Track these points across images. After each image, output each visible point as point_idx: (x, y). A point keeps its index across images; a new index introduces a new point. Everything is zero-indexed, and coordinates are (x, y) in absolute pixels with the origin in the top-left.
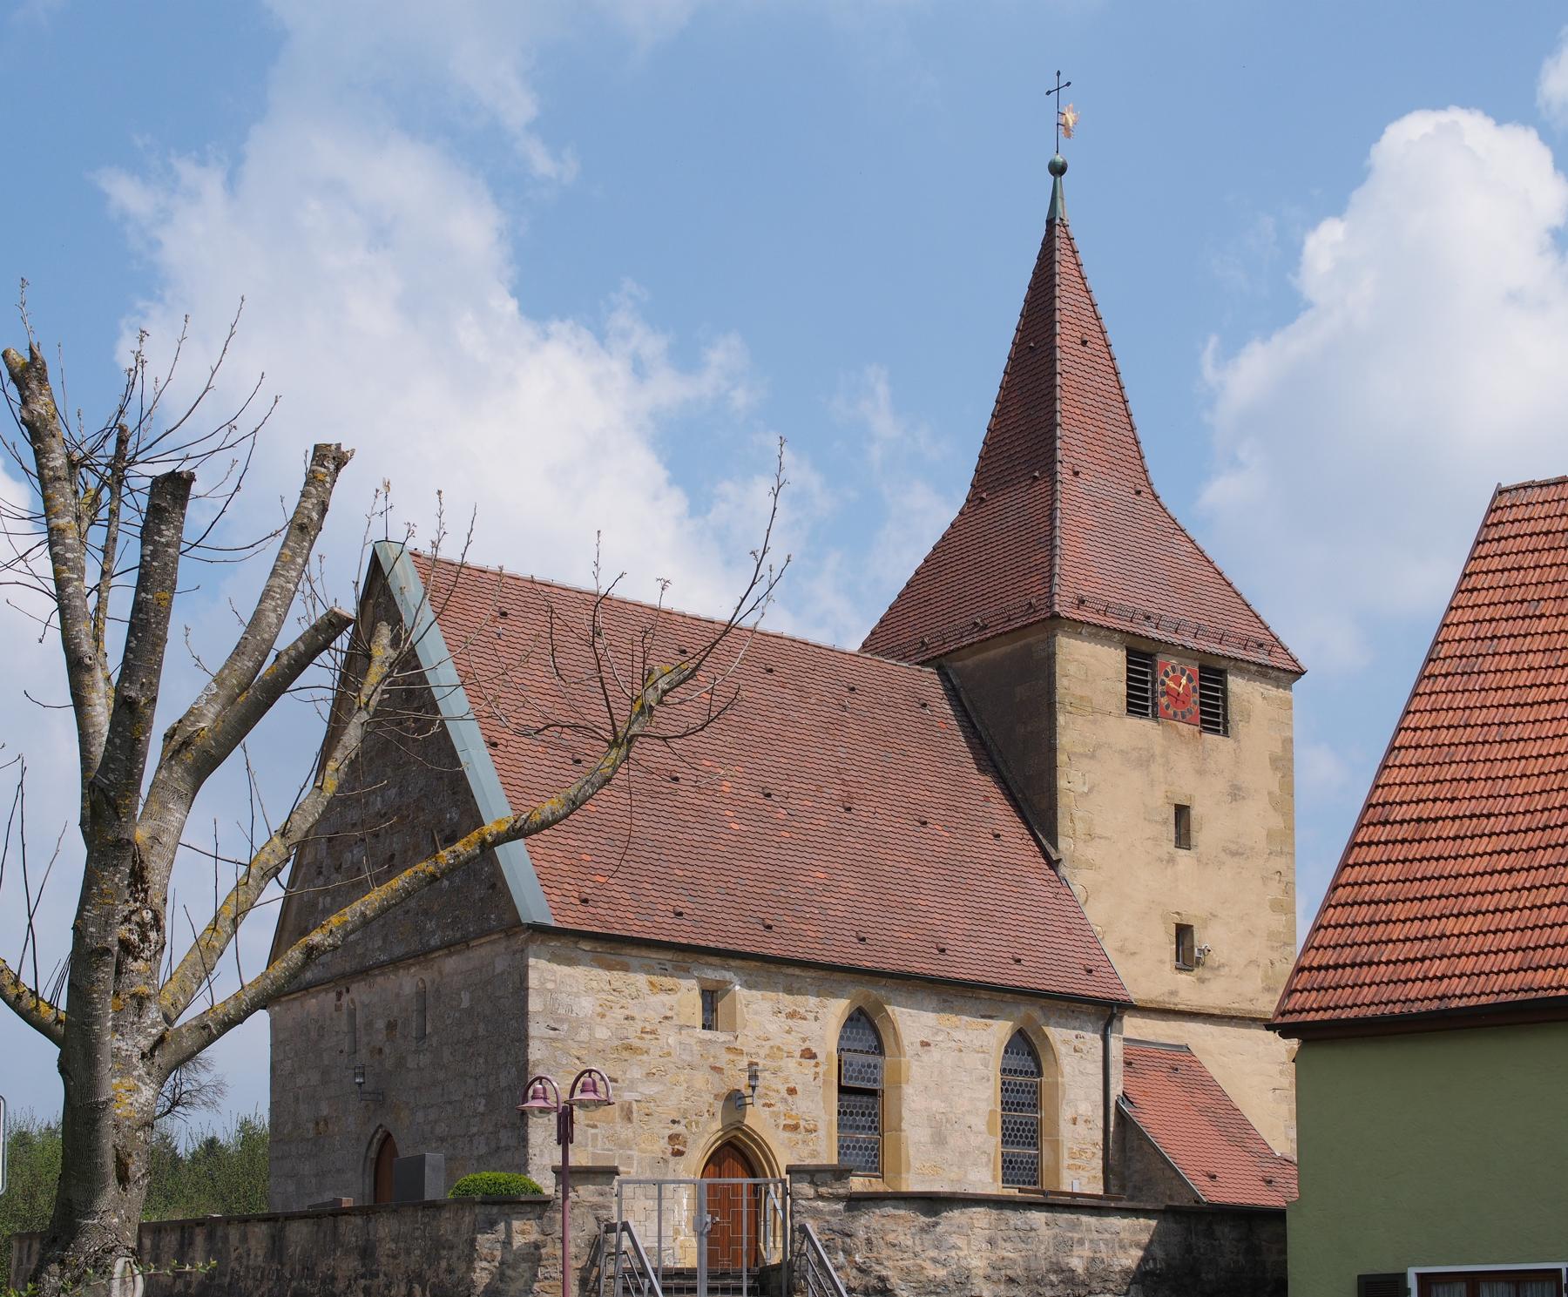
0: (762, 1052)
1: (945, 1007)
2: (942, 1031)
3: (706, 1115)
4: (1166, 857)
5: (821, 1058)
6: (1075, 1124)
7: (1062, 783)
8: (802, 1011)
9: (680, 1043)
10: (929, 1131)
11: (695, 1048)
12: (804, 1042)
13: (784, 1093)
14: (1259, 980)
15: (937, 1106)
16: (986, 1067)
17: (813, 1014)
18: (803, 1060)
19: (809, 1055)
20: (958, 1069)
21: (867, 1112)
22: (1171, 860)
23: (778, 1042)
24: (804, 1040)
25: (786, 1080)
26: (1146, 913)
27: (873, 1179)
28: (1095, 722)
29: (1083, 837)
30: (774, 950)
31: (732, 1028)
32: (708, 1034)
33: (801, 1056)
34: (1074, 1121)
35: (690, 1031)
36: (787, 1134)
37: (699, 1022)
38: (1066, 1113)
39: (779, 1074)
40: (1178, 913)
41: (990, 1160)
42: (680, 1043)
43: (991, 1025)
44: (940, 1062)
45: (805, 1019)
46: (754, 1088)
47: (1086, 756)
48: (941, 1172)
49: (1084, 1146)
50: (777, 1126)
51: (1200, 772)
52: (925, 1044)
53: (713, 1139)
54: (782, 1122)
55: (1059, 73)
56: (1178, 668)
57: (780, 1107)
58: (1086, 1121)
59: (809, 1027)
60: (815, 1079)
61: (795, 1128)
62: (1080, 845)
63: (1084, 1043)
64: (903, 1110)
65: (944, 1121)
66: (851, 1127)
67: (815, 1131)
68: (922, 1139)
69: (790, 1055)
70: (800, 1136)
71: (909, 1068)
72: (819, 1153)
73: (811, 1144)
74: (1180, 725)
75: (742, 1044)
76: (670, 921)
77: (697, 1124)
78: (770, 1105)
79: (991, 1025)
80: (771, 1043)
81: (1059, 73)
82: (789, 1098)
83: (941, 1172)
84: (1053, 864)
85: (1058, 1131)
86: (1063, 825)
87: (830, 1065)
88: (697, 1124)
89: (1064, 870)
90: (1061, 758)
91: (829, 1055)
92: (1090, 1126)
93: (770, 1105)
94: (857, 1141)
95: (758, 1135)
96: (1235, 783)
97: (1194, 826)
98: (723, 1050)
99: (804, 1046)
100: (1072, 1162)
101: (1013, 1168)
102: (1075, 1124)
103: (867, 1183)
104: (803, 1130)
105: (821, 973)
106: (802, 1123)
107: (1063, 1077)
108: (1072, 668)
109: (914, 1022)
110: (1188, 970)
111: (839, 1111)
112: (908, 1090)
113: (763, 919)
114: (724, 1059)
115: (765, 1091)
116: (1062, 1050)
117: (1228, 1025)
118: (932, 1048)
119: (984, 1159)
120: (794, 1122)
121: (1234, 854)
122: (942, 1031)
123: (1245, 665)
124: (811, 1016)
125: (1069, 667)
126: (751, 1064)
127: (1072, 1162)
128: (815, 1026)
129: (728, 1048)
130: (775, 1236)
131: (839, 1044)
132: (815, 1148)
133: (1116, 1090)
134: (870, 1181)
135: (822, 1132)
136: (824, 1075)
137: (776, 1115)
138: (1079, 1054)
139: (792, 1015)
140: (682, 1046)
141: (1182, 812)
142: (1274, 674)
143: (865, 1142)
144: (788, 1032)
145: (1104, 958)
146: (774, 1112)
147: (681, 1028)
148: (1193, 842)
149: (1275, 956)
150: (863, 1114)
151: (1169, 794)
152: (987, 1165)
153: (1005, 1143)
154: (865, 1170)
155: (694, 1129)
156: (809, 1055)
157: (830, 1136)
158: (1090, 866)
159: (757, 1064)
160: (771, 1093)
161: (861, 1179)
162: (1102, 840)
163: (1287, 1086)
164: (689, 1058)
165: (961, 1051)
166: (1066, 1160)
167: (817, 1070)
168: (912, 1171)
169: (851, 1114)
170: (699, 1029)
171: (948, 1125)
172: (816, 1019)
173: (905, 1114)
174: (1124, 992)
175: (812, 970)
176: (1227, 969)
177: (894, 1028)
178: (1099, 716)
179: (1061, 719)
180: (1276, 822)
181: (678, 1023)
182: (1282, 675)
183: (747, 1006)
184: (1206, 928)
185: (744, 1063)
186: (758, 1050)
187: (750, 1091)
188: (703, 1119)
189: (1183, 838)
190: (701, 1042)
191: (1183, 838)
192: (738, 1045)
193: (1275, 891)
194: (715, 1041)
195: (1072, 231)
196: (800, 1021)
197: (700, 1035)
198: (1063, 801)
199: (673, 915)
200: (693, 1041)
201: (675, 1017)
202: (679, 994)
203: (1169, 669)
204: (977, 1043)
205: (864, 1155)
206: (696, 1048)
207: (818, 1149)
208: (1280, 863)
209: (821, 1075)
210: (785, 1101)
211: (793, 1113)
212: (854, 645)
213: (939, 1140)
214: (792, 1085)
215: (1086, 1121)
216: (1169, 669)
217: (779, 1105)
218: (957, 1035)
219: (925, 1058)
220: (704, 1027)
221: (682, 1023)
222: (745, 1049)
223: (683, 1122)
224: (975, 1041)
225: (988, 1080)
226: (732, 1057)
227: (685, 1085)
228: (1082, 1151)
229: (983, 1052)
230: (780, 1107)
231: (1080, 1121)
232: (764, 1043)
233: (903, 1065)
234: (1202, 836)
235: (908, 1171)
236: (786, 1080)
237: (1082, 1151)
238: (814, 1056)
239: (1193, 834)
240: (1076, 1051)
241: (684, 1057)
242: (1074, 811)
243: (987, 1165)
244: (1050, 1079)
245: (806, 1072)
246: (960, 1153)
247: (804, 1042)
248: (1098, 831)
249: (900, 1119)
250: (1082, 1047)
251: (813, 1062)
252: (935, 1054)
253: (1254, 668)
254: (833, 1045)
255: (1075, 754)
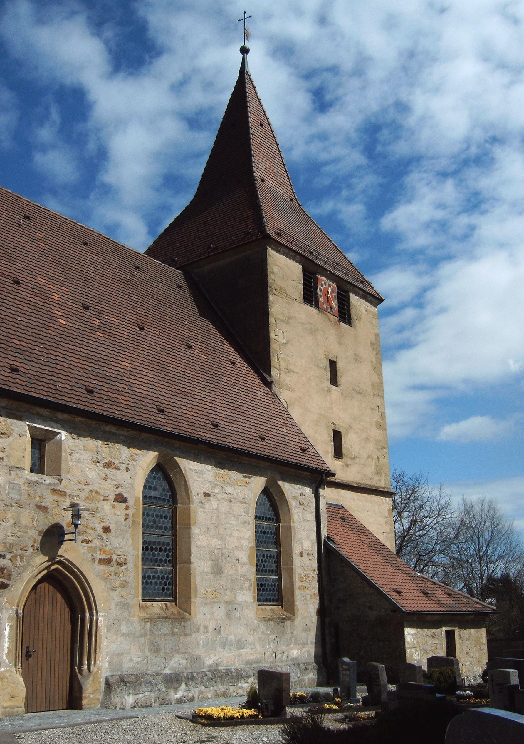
0: (83, 495)
1: (220, 464)
2: (218, 485)
3: (31, 550)
4: (326, 389)
5: (131, 502)
6: (301, 556)
7: (272, 335)
8: (116, 462)
9: (10, 483)
10: (210, 563)
11: (23, 487)
12: (117, 488)
13: (100, 531)
14: (373, 469)
15: (216, 543)
16: (247, 514)
17: (126, 466)
18: (116, 503)
19: (121, 499)
20: (229, 515)
21: (163, 548)
22: (329, 391)
23: (96, 487)
24: (117, 487)
25: (102, 520)
26: (318, 422)
27: (168, 603)
28: (288, 303)
29: (284, 370)
30: (96, 408)
31: (57, 472)
32: (35, 477)
33: (115, 500)
34: (301, 554)
35: (18, 472)
36: (102, 567)
37: (27, 463)
38: (296, 549)
39: (96, 514)
40: (77, 515)
41: (251, 585)
42: (10, 483)
43: (249, 483)
44: (217, 509)
45: (118, 469)
46: (76, 526)
47: (284, 322)
48: (219, 596)
49: (308, 572)
50: (94, 560)
51: (340, 343)
52: (207, 495)
53: (36, 571)
54: (98, 556)
55: (245, 13)
56: (327, 284)
57: (96, 543)
58: (308, 554)
59: (122, 476)
60: (125, 520)
61: (108, 561)
62: (283, 374)
63: (305, 499)
64: (192, 547)
65: (220, 555)
66: (151, 560)
67: (125, 564)
68: (206, 570)
69: (106, 499)
70: (112, 569)
71: (196, 513)
72: (127, 583)
73: (121, 575)
74: (330, 315)
75: (65, 487)
76: (7, 375)
77: (22, 558)
78: (87, 542)
79: (249, 483)
80: (91, 487)
81: (245, 13)
82: (105, 536)
83: (219, 596)
84: (269, 384)
85: (292, 561)
86: (274, 361)
87: (138, 509)
88: (22, 558)
89: (275, 389)
90: (272, 320)
91: (136, 501)
92: (310, 558)
93: (87, 542)
94: (156, 572)
95: (77, 568)
96: (356, 353)
97: (339, 374)
98: (49, 492)
99: (118, 491)
100: (301, 584)
101: (263, 590)
102: (301, 556)
103: (164, 607)
104: (115, 564)
105: (133, 433)
106: (115, 557)
107: (294, 523)
108: (276, 269)
109: (199, 477)
110: (340, 459)
111: (143, 547)
112: (195, 530)
113: (86, 386)
114: (49, 499)
115: (84, 529)
116: (293, 503)
117: (361, 492)
118: (212, 498)
119: (247, 584)
120: (108, 556)
121: (359, 393)
122: (218, 485)
123: (357, 290)
124: (123, 467)
125: (274, 268)
126: (73, 505)
127: (301, 584)
128: (127, 476)
129: (53, 490)
130: (3, 190)
131: (143, 492)
132: (124, 579)
133: (324, 532)
134: (166, 605)
135: (130, 565)
136: (133, 516)
137: (93, 550)
138: (303, 507)
139: (108, 465)
140: (11, 486)
141: (333, 364)
142: (370, 298)
143: (161, 573)
144: (105, 479)
145: (309, 443)
146: (91, 547)
147: (11, 468)
148: (339, 383)
149: (379, 454)
150: (161, 550)
151: (326, 353)
152: (249, 589)
153: (258, 571)
154: (162, 596)
155: (19, 563)
156: (121, 499)
157: (136, 566)
158: (289, 389)
159: (78, 504)
160: (89, 531)
161: (159, 603)
162: (295, 374)
163: (388, 531)
164: (17, 497)
165: (231, 501)
166: (297, 583)
167: (127, 512)
168: (199, 595)
169: (152, 549)
170: (27, 472)
171: (223, 558)
172: (127, 469)
173: (194, 549)
174: (325, 465)
175: (126, 429)
176: (358, 460)
177: (185, 481)
178: (290, 300)
179: (271, 297)
180: (375, 378)
181: (8, 464)
182: (373, 299)
183: (71, 454)
184: (347, 434)
185: (67, 503)
186: (79, 493)
187: (72, 528)
188: (27, 553)
189: (334, 380)
190: (30, 483)
191: (334, 380)
192: (61, 487)
193: (377, 418)
194: (42, 483)
195: (252, 77)
196: (114, 471)
197: (28, 477)
198: (274, 346)
199: (9, 371)
200: (21, 482)
201: (6, 459)
202: (11, 438)
203: (323, 283)
204: (241, 496)
205: (161, 583)
206: (24, 488)
207: (127, 579)
208: (378, 401)
209: (130, 517)
210: (100, 537)
211: (107, 549)
212: (142, 250)
213: (217, 570)
214: (106, 524)
215: (308, 554)
216: (323, 283)
217: (95, 541)
218: (229, 489)
219: (207, 506)
220: (32, 471)
221: (13, 464)
222: (68, 492)
223: (9, 556)
224: (240, 494)
225: (249, 524)
226: (56, 498)
227: (12, 522)
228: (307, 576)
229: (245, 503)
230: (96, 543)
231: (304, 554)
232: (85, 487)
233: (191, 510)
234: (342, 379)
235: (196, 597)
236: (102, 520)
237: (307, 576)
238: (125, 500)
239: (339, 378)
240: (300, 504)
241: (12, 495)
242: (279, 353)
243: (249, 589)
244: (285, 524)
245: (119, 514)
246: (232, 580)
247: (117, 488)
248: (292, 368)
249: (189, 554)
250: (305, 502)
251: (124, 505)
252: (214, 503)
253: (361, 292)
254: (139, 491)
255: (278, 319)
